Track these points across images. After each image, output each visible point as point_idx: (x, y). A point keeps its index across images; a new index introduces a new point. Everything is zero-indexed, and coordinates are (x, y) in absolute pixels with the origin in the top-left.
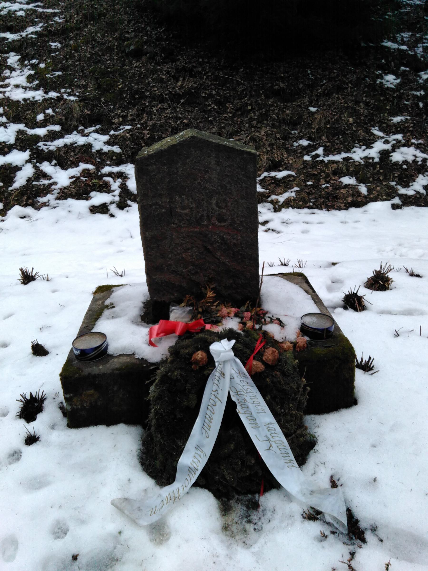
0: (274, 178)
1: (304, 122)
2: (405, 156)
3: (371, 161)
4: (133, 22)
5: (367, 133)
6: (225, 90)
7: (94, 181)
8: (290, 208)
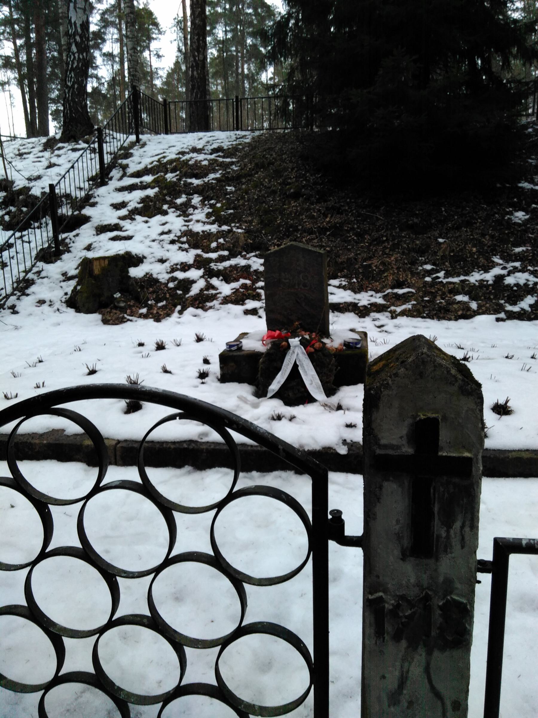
0: (396, 294)
1: (432, 251)
2: (517, 280)
3: (485, 283)
4: (296, 169)
5: (487, 260)
6: (365, 225)
7: (250, 292)
8: (405, 317)
